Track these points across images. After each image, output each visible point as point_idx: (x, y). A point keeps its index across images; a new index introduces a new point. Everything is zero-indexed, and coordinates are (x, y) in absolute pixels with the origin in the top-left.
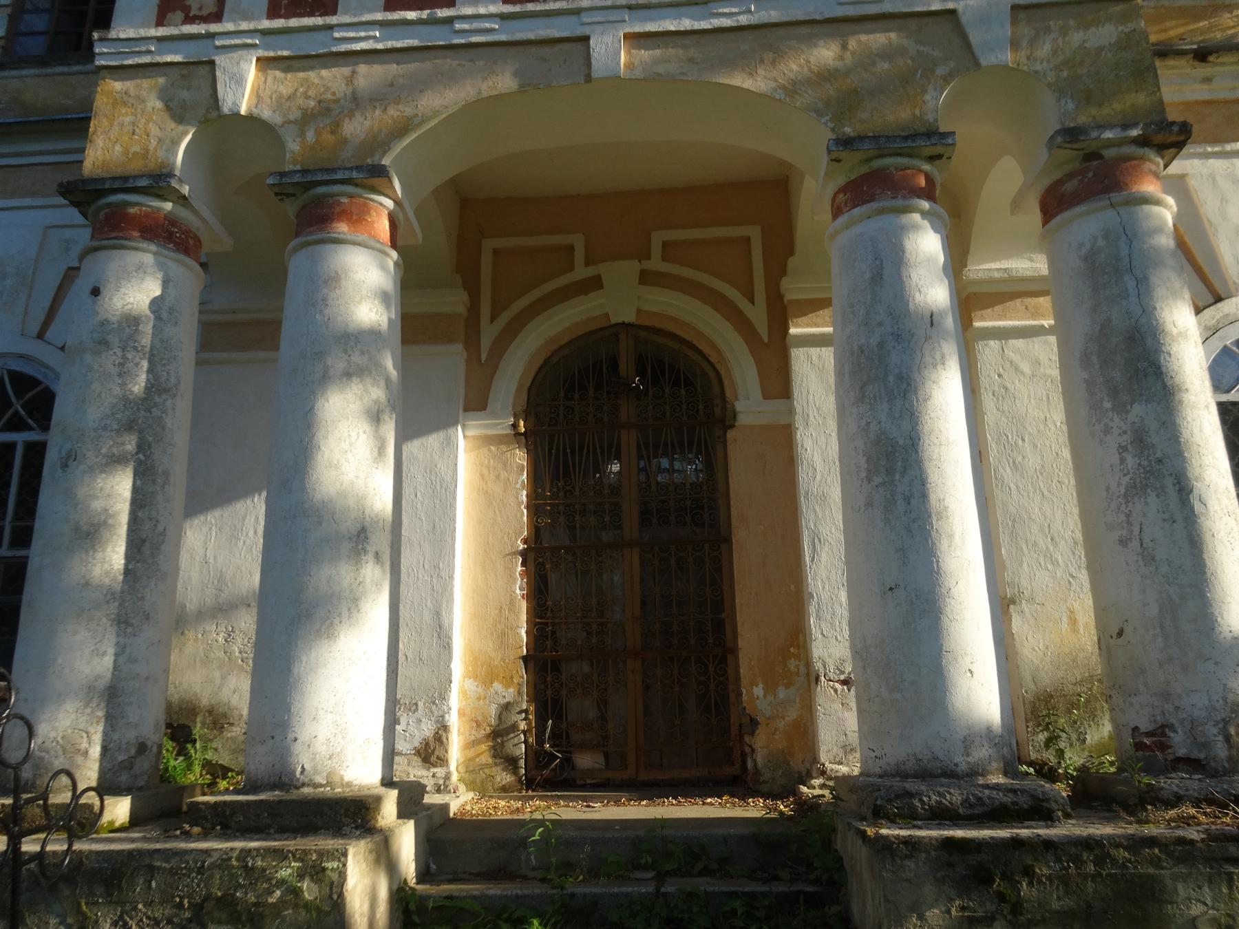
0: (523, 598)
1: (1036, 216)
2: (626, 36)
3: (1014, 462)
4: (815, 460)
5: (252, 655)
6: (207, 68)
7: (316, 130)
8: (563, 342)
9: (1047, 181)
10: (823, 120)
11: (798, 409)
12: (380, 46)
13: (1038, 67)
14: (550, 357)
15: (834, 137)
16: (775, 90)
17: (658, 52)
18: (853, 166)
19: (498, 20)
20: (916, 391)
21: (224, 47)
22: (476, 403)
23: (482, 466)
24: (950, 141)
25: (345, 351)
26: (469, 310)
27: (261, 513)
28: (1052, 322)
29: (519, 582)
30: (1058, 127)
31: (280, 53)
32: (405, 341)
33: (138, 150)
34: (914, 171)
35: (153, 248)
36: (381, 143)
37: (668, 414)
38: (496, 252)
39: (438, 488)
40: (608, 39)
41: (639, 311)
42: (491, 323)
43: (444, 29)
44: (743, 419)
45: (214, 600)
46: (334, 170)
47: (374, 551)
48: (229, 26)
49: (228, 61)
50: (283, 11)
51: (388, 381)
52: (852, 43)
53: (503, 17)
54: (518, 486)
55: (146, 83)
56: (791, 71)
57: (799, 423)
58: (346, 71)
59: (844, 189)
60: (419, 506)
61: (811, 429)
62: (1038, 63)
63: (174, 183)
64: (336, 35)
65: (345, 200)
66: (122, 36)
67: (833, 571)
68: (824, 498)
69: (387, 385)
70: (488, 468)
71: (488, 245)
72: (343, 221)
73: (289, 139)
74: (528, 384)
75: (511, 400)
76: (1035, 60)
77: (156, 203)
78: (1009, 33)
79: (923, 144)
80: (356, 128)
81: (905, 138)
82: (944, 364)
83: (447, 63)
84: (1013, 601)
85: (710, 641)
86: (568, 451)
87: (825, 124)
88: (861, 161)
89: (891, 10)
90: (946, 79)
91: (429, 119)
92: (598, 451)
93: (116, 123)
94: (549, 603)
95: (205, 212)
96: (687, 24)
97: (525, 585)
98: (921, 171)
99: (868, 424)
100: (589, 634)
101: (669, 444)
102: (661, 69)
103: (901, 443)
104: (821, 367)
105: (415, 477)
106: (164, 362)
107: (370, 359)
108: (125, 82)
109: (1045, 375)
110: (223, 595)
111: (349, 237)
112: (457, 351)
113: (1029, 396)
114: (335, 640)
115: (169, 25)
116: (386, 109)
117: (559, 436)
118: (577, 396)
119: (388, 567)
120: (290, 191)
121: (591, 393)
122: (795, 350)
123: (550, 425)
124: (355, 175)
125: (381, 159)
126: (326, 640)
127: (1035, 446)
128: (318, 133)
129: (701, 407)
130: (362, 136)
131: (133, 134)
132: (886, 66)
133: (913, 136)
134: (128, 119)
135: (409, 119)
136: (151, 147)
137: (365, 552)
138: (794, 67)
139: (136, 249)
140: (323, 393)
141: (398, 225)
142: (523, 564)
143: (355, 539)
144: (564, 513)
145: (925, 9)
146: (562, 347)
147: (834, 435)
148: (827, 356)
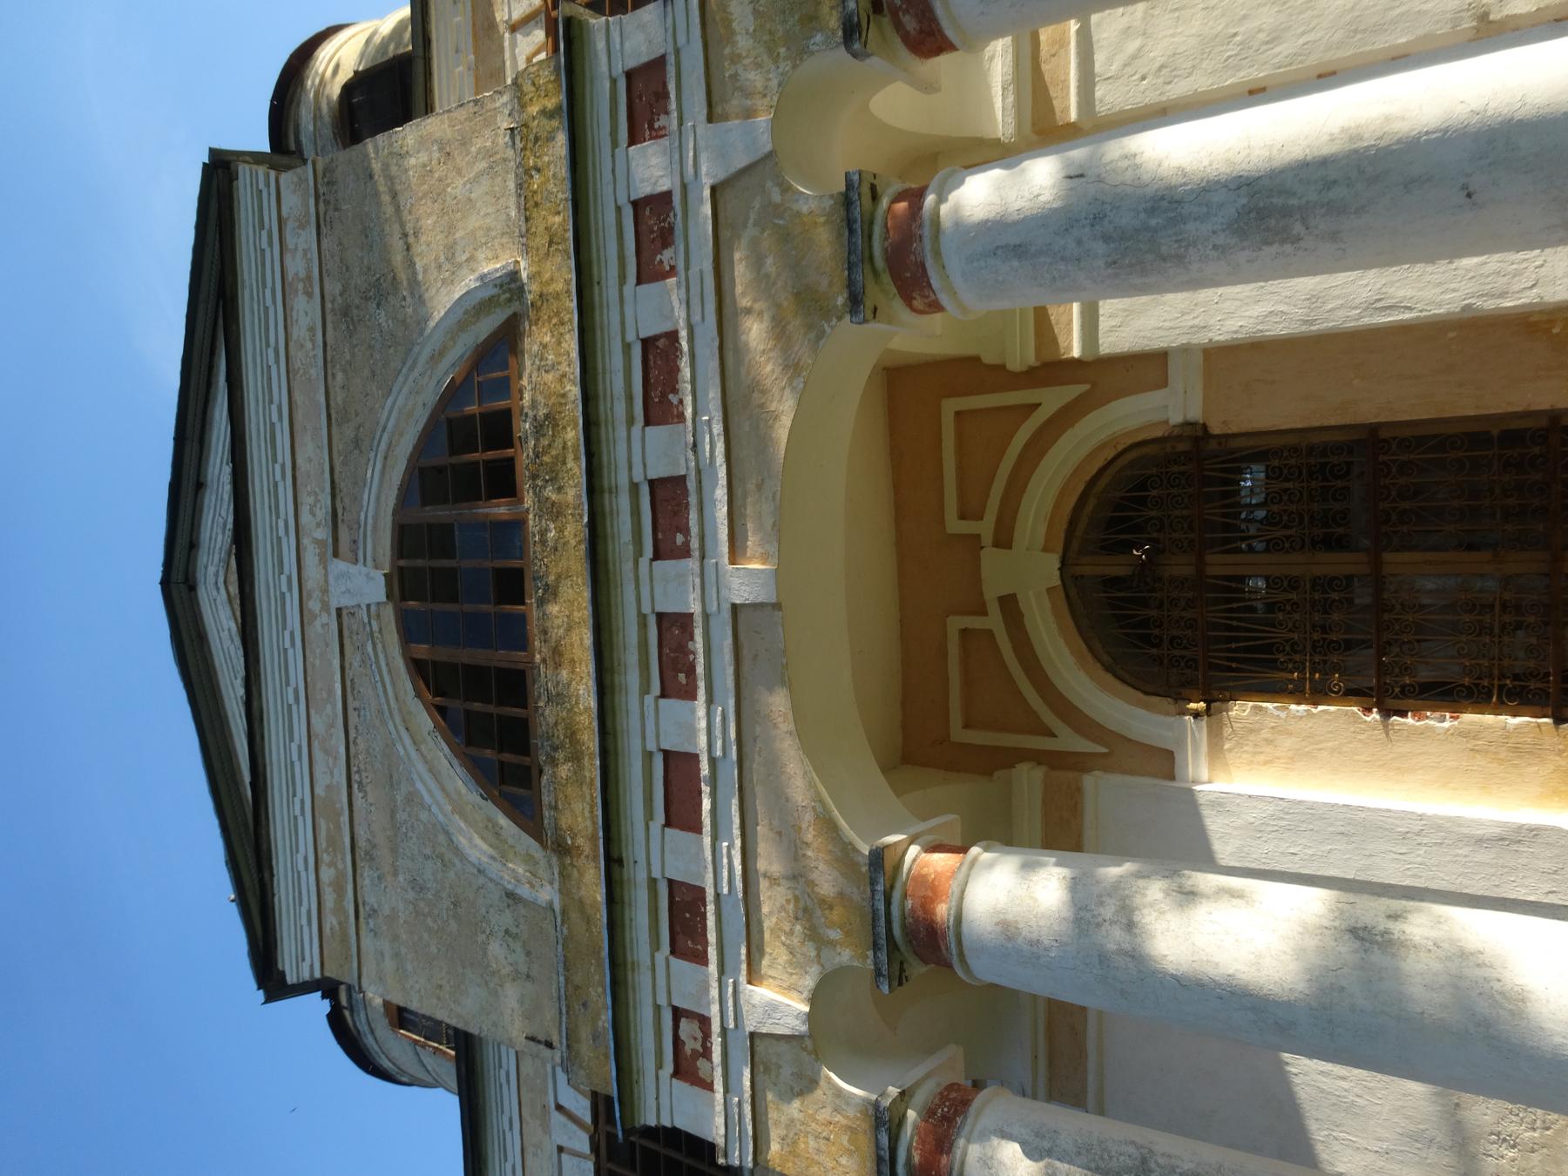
0: (1458, 717)
1: (944, 60)
2: (732, 562)
3: (1267, 43)
4: (1257, 314)
5: (1540, 1112)
6: (757, 1042)
7: (828, 927)
8: (1084, 647)
9: (903, 52)
10: (828, 330)
11: (1183, 340)
12: (738, 843)
13: (774, 83)
14: (1103, 665)
15: (848, 317)
16: (793, 389)
17: (750, 526)
18: (882, 292)
19: (712, 707)
20: (1170, 188)
21: (736, 1019)
22: (1164, 763)
23: (1252, 762)
24: (856, 177)
25: (1098, 925)
26: (1039, 764)
27: (1315, 1067)
28: (1072, 22)
29: (1432, 722)
30: (843, 48)
31: (743, 957)
32: (1078, 847)
33: (847, 1137)
34: (889, 217)
35: (961, 1142)
36: (844, 854)
37: (1185, 512)
38: (967, 726)
39: (1284, 823)
40: (735, 582)
41: (1045, 549)
42: (1056, 736)
43: (720, 766)
44: (1195, 413)
45: (1446, 1153)
46: (875, 912)
47: (1386, 920)
48: (714, 1010)
49: (750, 1017)
50: (699, 947)
51: (1139, 875)
52: (744, 302)
53: (710, 701)
54: (1283, 715)
55: (773, 1115)
56: (773, 370)
57: (1202, 338)
58: (764, 884)
59: (908, 300)
60: (1310, 852)
61: (1211, 322)
62: (770, 84)
63: (886, 1103)
64: (725, 891)
65: (909, 903)
66: (722, 1131)
67: (1428, 278)
68: (1313, 299)
69: (1144, 877)
70: (1255, 754)
71: (959, 734)
72: (934, 909)
73: (837, 960)
74: (1140, 695)
75: (1162, 718)
76: (766, 87)
77: (908, 1129)
78: (737, 122)
79: (858, 209)
80: (827, 881)
81: (851, 231)
82: (1135, 155)
83: (756, 765)
84: (1483, 17)
85: (1536, 450)
86: (1233, 646)
87: (832, 327)
88: (876, 283)
89: (711, 260)
90: (786, 189)
91: (818, 794)
92: (1235, 605)
93: (816, 1157)
94: (1467, 681)
95: (918, 1072)
96: (721, 493)
97: (1437, 714)
98: (889, 208)
99: (1215, 247)
100: (1519, 626)
101: (1224, 511)
102: (769, 522)
103: (1244, 201)
104: (1125, 314)
105: (1263, 853)
106: (1106, 1156)
107: (1110, 895)
108: (772, 1138)
109: (1144, 19)
110: (1439, 1139)
111: (954, 903)
112: (1090, 782)
113: (1173, 35)
114: (1529, 992)
115: (712, 1075)
116: (806, 843)
117: (1210, 657)
118: (1156, 632)
119: (1411, 904)
120: (897, 967)
121: (1154, 613)
122: (1101, 349)
123: (1196, 669)
124: (880, 888)
125: (862, 854)
126: (1528, 1004)
127: (1245, 17)
128: (832, 925)
129: (1175, 469)
130: (835, 873)
131: (828, 1139)
132: (770, 261)
133: (850, 223)
134: (812, 1143)
135: (817, 817)
136: (844, 1122)
137: (1387, 933)
138: (769, 368)
139: (963, 1163)
140: (1155, 961)
141: (938, 842)
142: (1403, 714)
143: (1367, 944)
144: (1325, 655)
145: (710, 222)
146: (1090, 649)
147: (1220, 290)
148: (1109, 308)
